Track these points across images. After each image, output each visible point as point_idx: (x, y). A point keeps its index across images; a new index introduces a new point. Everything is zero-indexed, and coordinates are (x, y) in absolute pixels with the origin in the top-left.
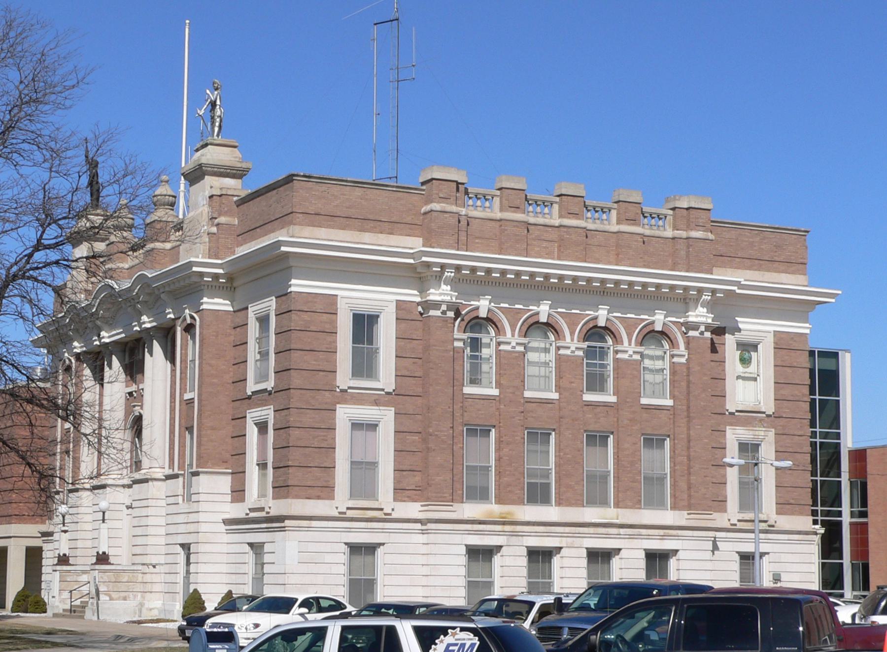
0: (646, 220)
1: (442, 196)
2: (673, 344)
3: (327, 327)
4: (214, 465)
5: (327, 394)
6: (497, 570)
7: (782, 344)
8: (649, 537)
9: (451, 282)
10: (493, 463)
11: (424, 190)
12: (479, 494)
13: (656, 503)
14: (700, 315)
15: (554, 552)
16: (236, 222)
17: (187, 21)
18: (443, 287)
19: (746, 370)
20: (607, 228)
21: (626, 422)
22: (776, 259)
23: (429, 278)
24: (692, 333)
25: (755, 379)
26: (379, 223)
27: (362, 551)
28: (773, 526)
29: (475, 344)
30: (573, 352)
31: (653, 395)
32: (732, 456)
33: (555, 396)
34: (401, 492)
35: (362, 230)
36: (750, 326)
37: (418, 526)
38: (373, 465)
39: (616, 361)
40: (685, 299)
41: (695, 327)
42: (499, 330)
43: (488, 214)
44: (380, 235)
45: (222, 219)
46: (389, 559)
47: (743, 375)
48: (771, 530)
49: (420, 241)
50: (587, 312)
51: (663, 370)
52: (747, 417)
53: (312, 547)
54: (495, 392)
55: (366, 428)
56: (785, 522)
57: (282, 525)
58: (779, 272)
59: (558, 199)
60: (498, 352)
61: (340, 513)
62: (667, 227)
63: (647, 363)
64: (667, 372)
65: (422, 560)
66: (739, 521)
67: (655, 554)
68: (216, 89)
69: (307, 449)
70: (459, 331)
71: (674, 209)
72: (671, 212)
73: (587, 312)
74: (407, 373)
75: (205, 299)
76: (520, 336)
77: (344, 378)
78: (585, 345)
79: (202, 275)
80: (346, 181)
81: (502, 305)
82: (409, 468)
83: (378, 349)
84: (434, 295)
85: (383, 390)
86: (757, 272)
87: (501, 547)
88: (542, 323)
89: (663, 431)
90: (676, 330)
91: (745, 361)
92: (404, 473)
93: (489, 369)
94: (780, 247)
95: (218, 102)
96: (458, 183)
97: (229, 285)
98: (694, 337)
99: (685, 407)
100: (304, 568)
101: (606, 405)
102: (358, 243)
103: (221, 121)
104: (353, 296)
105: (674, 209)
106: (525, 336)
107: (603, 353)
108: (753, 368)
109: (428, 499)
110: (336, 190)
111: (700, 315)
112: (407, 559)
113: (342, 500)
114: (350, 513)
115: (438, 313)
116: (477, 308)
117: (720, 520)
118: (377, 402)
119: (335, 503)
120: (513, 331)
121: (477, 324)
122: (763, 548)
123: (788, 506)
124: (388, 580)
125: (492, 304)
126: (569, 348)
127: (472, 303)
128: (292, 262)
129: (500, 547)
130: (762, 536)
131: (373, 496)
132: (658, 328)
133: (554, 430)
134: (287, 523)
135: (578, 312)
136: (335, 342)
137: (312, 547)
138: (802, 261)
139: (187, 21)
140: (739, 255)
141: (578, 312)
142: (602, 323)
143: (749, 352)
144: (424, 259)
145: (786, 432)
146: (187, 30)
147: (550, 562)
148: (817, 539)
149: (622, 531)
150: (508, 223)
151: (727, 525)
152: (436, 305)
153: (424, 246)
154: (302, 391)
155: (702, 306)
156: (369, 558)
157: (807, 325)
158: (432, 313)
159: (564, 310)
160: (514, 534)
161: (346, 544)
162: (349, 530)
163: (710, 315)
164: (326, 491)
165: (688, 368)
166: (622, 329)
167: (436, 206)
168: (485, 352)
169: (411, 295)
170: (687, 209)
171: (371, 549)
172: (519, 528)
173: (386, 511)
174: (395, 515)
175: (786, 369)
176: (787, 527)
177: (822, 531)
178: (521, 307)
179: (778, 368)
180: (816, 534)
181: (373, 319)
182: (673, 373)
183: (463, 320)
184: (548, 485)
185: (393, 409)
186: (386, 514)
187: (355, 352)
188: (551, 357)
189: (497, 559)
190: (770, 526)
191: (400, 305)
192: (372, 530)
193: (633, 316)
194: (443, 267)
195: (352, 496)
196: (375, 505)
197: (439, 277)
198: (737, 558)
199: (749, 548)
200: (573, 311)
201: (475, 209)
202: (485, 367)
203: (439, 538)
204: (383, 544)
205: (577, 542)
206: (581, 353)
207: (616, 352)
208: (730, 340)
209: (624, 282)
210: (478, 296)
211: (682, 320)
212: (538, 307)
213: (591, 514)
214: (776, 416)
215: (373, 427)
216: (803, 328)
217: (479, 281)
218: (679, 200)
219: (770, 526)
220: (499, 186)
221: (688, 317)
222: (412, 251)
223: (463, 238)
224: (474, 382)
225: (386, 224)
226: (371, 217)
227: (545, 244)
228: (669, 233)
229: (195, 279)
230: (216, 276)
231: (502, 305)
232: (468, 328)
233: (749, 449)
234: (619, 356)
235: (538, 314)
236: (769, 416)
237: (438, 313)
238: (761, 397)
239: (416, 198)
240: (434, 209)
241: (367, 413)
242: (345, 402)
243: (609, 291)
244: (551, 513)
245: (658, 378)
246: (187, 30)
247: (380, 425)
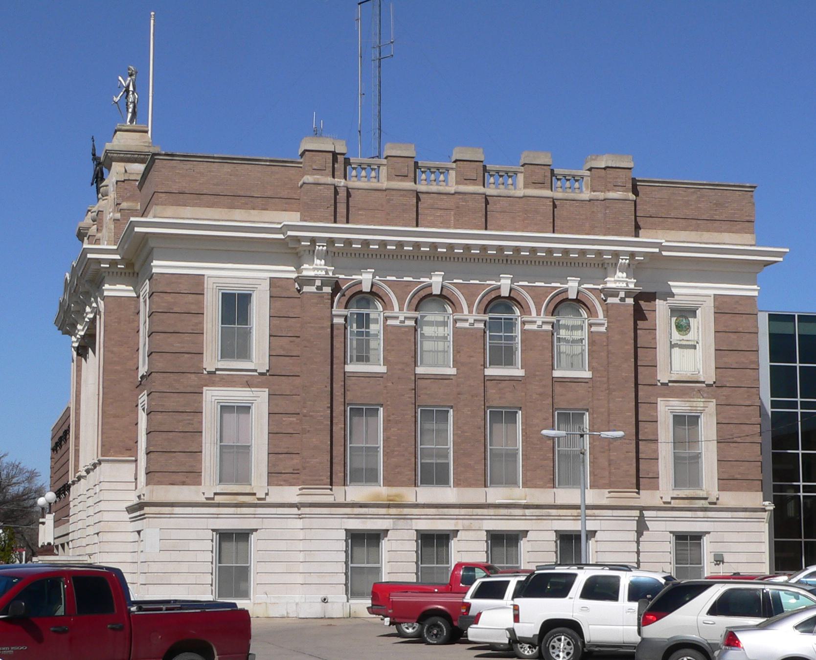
0: (559, 182)
1: (315, 167)
2: (592, 312)
3: (193, 308)
4: (117, 453)
5: (193, 376)
6: (385, 556)
7: (725, 309)
8: (559, 518)
9: (627, 269)
10: (381, 444)
11: (301, 163)
12: (368, 476)
13: (572, 481)
14: (619, 280)
15: (382, 535)
16: (139, 208)
17: (152, 13)
18: (317, 261)
19: (685, 338)
20: (512, 192)
21: (535, 396)
22: (717, 217)
23: (302, 253)
24: (610, 300)
25: (694, 347)
26: (251, 199)
27: (232, 539)
28: (715, 504)
29: (363, 321)
30: (402, 322)
31: (572, 367)
32: (665, 432)
33: (452, 371)
34: (275, 476)
35: (232, 207)
36: (684, 290)
37: (295, 510)
38: (245, 450)
39: (524, 332)
40: (603, 265)
41: (614, 293)
42: (387, 305)
43: (374, 184)
44: (252, 211)
45: (124, 205)
46: (262, 545)
47: (679, 343)
48: (713, 506)
49: (298, 215)
50: (488, 282)
51: (581, 340)
52: (684, 387)
53: (175, 534)
54: (382, 369)
55: (239, 408)
56: (729, 499)
57: (142, 512)
58: (721, 232)
59: (454, 165)
60: (385, 327)
61: (665, 503)
62: (584, 189)
63: (563, 333)
64: (586, 342)
65: (301, 546)
66: (673, 498)
67: (433, 535)
68: (131, 75)
69: (171, 434)
70: (338, 307)
71: (590, 170)
72: (588, 173)
73: (488, 282)
74: (283, 353)
75: (107, 286)
76: (408, 310)
77: (212, 360)
78: (486, 317)
79: (99, 261)
80: (214, 158)
81: (389, 278)
82: (286, 451)
83: (250, 328)
84: (308, 271)
85: (256, 371)
86: (694, 233)
87: (388, 530)
88: (435, 295)
89: (580, 405)
90: (594, 297)
91: (683, 328)
92: (281, 456)
93: (378, 345)
94: (722, 204)
95: (131, 88)
96: (335, 155)
97: (130, 271)
98: (613, 304)
99: (605, 379)
100: (166, 556)
101: (512, 379)
102: (219, 220)
103: (134, 107)
104: (221, 275)
105: (590, 170)
106: (346, 308)
107: (510, 325)
108: (691, 336)
109: (304, 483)
110: (203, 167)
111: (619, 280)
112: (282, 545)
113: (209, 486)
114: (675, 504)
115: (313, 289)
116: (360, 282)
117: (646, 497)
118: (249, 384)
119: (202, 488)
120: (470, 306)
121: (363, 298)
122: (591, 526)
123: (732, 482)
124: (261, 567)
125: (377, 278)
126: (467, 320)
127: (354, 277)
128: (152, 243)
129: (456, 532)
130: (589, 512)
131: (247, 480)
132: (572, 295)
133: (452, 407)
134: (147, 510)
135: (477, 282)
136: (202, 323)
137: (175, 534)
138: (748, 218)
139: (152, 13)
140: (672, 215)
141: (477, 282)
142: (505, 293)
143: (686, 318)
144: (290, 233)
145: (730, 401)
146: (152, 21)
147: (447, 546)
148: (765, 515)
149: (528, 512)
150: (394, 193)
151: (659, 503)
152: (310, 281)
153: (302, 220)
154: (165, 375)
155: (621, 271)
156: (241, 545)
157: (755, 287)
158: (306, 289)
159: (461, 281)
160: (403, 517)
161: (671, 532)
162: (217, 516)
163: (633, 280)
164: (193, 476)
165: (608, 338)
166: (529, 298)
167: (308, 179)
168: (374, 328)
169: (287, 272)
170: (605, 169)
171: (243, 536)
172: (406, 511)
173: (258, 496)
174: (269, 500)
175: (730, 334)
176: (732, 504)
177: (772, 507)
178: (411, 279)
179: (718, 334)
180: (764, 510)
181: (245, 299)
182: (592, 343)
183: (344, 295)
184: (448, 464)
185: (714, 400)
186: (259, 499)
187: (225, 334)
188: (449, 331)
189: (385, 544)
190: (710, 503)
191: (274, 282)
192: (243, 516)
193: (542, 284)
194: (313, 241)
195: (677, 484)
196: (247, 489)
197: (311, 252)
198: (672, 538)
199: (570, 526)
200: (537, 284)
201: (359, 180)
202: (373, 344)
203: (316, 523)
204: (256, 530)
205: (476, 524)
206: (482, 326)
207: (524, 323)
208: (661, 307)
209: (476, 246)
210: (359, 270)
211: (600, 287)
212: (431, 279)
213: (496, 494)
214: (717, 386)
215: (246, 409)
216: (750, 290)
217: (357, 254)
218: (594, 160)
219: (710, 503)
220: (522, 162)
221: (606, 283)
222: (280, 226)
223: (342, 209)
224: (363, 358)
225: (259, 199)
226: (242, 193)
227: (439, 213)
228: (586, 195)
229: (93, 267)
230: (113, 263)
231: (389, 278)
232: (488, 310)
233: (686, 423)
234: (527, 327)
235: (430, 286)
236: (708, 386)
237: (313, 289)
238: (700, 366)
239: (293, 171)
240: (306, 181)
241: (237, 395)
242: (213, 384)
243: (607, 262)
244: (448, 494)
245: (441, 345)
246: (152, 21)
247: (253, 408)
